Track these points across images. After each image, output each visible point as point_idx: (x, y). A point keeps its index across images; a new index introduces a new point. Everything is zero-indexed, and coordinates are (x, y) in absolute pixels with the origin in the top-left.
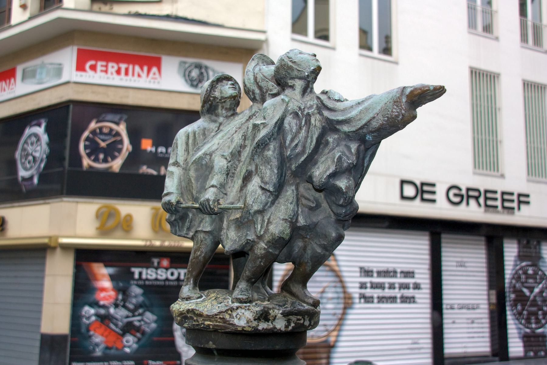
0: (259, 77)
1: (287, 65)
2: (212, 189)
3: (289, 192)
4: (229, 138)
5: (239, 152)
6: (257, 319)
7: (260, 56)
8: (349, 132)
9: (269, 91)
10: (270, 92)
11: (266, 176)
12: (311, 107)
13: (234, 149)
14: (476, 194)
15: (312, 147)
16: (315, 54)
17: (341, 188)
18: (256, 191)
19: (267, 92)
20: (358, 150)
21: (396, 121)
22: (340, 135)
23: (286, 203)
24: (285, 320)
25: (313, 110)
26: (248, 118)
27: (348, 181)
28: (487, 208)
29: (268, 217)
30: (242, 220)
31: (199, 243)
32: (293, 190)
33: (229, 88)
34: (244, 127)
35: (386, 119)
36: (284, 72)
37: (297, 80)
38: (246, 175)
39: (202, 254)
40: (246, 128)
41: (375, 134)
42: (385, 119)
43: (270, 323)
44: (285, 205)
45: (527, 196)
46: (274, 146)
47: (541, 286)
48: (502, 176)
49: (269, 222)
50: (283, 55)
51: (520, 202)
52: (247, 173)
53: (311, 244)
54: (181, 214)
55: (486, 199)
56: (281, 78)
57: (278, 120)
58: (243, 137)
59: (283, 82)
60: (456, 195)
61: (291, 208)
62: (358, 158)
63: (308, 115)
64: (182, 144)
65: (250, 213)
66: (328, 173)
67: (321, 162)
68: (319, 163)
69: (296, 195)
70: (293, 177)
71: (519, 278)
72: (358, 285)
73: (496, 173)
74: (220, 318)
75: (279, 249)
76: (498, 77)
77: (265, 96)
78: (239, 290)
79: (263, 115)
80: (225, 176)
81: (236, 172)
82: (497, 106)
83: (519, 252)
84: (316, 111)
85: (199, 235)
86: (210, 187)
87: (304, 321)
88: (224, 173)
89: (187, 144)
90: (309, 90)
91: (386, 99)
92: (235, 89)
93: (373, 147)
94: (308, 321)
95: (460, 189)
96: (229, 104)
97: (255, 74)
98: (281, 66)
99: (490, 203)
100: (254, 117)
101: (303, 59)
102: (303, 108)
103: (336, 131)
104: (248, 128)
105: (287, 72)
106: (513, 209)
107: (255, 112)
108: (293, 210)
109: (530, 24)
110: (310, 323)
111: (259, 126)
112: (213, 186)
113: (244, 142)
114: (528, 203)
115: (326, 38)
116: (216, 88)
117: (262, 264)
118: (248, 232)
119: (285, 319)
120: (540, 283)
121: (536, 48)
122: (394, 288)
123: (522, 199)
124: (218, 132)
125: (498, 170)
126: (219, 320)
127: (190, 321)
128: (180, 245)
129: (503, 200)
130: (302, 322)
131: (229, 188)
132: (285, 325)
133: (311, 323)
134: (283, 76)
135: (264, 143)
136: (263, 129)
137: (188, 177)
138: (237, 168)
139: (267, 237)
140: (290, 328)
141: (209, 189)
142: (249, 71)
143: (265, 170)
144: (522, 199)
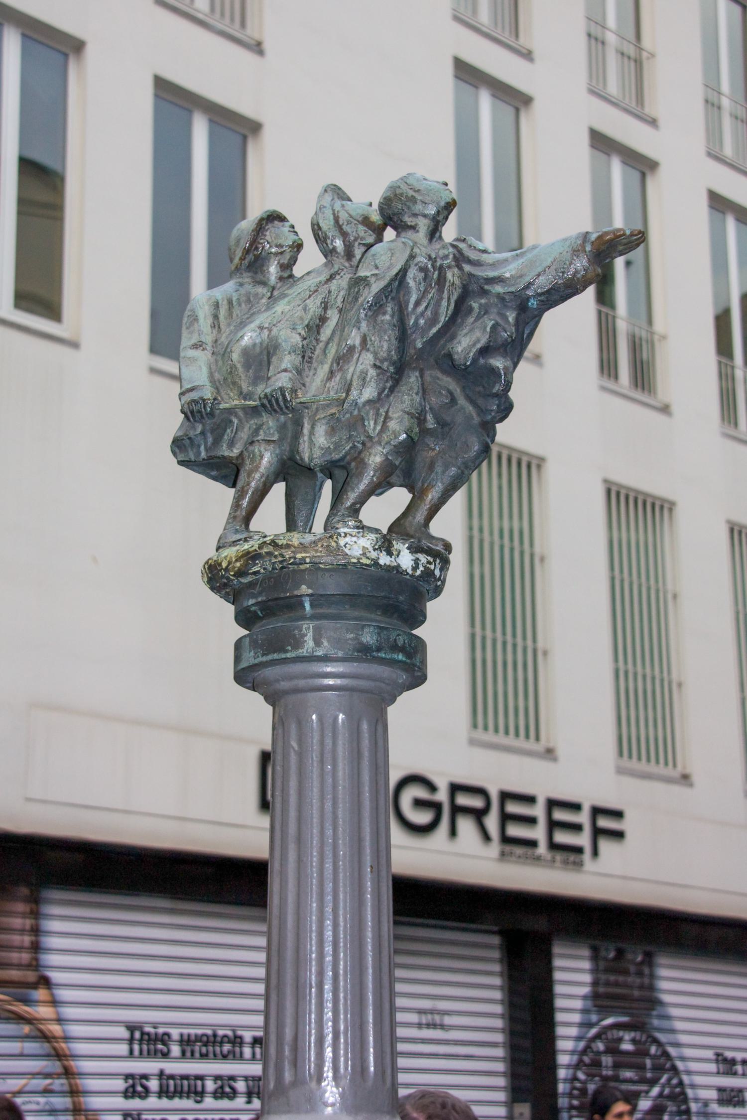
0: (343, 216)
1: (405, 194)
3: (412, 379)
4: (299, 306)
5: (318, 327)
6: (377, 549)
8: (504, 293)
10: (361, 240)
11: (382, 350)
12: (446, 257)
13: (311, 320)
14: (477, 802)
15: (450, 312)
16: (448, 182)
17: (498, 367)
20: (517, 320)
21: (575, 279)
22: (489, 299)
23: (411, 393)
24: (412, 560)
25: (449, 261)
26: (329, 277)
28: (508, 848)
29: (386, 409)
30: (342, 416)
31: (257, 460)
32: (416, 377)
34: (324, 290)
36: (400, 205)
37: (420, 218)
38: (345, 351)
40: (327, 292)
41: (542, 298)
43: (393, 559)
44: (408, 395)
45: (618, 814)
46: (392, 308)
47: (655, 1091)
48: (550, 753)
49: (387, 417)
50: (398, 181)
51: (598, 833)
52: (346, 348)
54: (217, 420)
55: (506, 818)
56: (394, 214)
57: (400, 271)
58: (323, 304)
59: (397, 221)
60: (419, 803)
61: (418, 401)
62: (517, 330)
63: (441, 268)
64: (205, 317)
65: (356, 404)
66: (479, 346)
67: (462, 335)
68: (459, 337)
69: (422, 384)
71: (596, 1064)
72: (120, 1084)
73: (531, 745)
75: (402, 457)
76: (539, 467)
77: (353, 246)
79: (373, 263)
80: (300, 358)
81: (315, 357)
82: (537, 549)
83: (595, 983)
84: (453, 263)
85: (255, 449)
86: (282, 372)
88: (299, 354)
89: (216, 317)
90: (437, 235)
93: (537, 319)
95: (432, 787)
96: (288, 257)
97: (336, 212)
98: (396, 195)
99: (514, 831)
100: (338, 277)
101: (432, 187)
102: (434, 257)
103: (484, 293)
104: (331, 292)
105: (406, 204)
106: (579, 850)
107: (339, 269)
108: (420, 404)
109: (622, 326)
111: (368, 279)
112: (285, 370)
113: (325, 312)
114: (618, 835)
115: (52, 310)
116: (267, 231)
117: (375, 480)
120: (653, 1082)
121: (638, 395)
122: (234, 1094)
123: (604, 823)
125: (538, 738)
127: (265, 560)
129: (553, 825)
131: (307, 377)
132: (412, 566)
135: (379, 303)
136: (375, 282)
137: (230, 362)
138: (315, 350)
142: (324, 207)
143: (380, 342)
144: (604, 823)
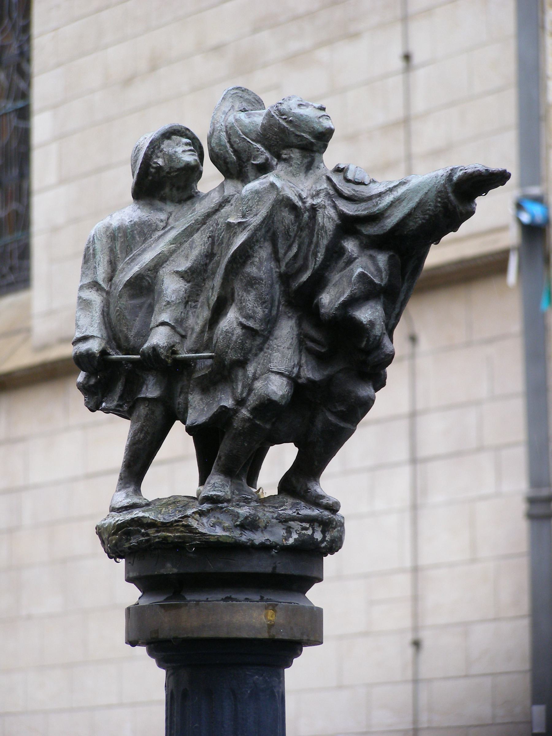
2: (163, 331)
7: (235, 91)
9: (252, 159)
10: (254, 160)
18: (233, 331)
19: (248, 160)
24: (284, 529)
27: (373, 312)
33: (184, 151)
35: (427, 216)
39: (147, 437)
42: (426, 217)
53: (323, 411)
70: (178, 354)
74: (183, 526)
78: (210, 486)
86: (157, 326)
87: (313, 532)
91: (427, 186)
92: (193, 153)
94: (320, 532)
110: (324, 537)
112: (163, 324)
118: (223, 396)
119: (283, 527)
124: (166, 229)
126: (181, 529)
128: (357, 206)
130: (310, 532)
133: (326, 537)
134: (273, 143)
139: (252, 401)
140: (291, 541)
141: (157, 328)
